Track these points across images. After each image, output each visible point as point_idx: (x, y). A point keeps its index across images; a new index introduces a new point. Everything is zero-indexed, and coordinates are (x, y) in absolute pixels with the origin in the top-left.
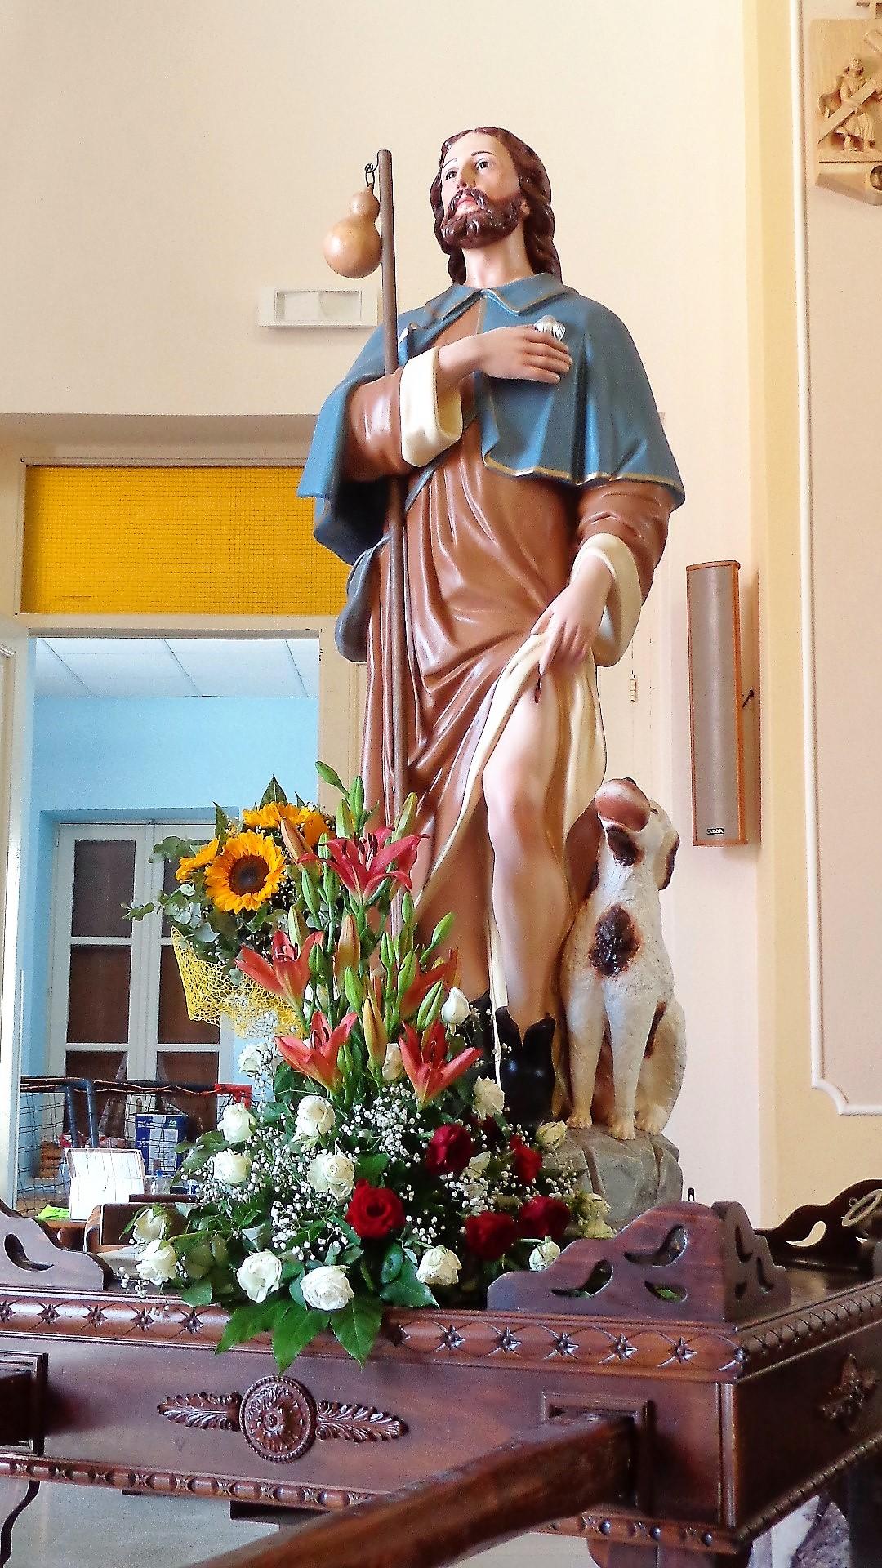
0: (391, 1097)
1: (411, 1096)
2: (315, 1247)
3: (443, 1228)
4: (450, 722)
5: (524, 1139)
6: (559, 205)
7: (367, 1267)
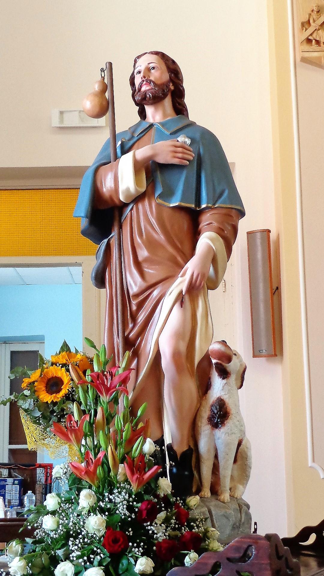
0: (121, 489)
2: (89, 558)
3: (146, 547)
5: (181, 505)
6: (186, 85)
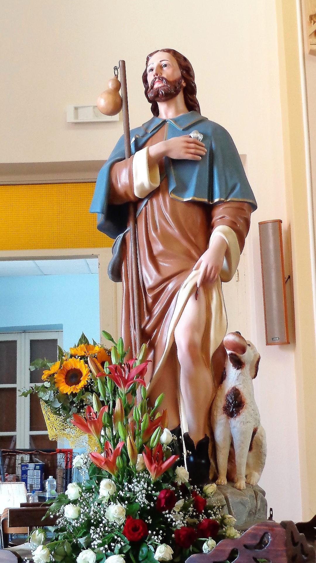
1: (149, 477)
2: (110, 546)
4: (160, 308)
5: (198, 492)
6: (198, 81)
7: (133, 553)
